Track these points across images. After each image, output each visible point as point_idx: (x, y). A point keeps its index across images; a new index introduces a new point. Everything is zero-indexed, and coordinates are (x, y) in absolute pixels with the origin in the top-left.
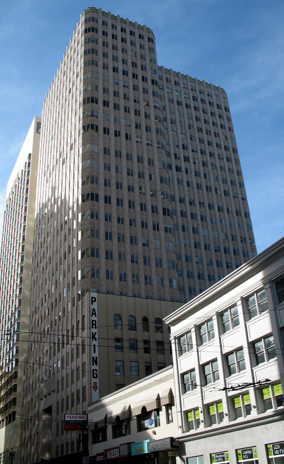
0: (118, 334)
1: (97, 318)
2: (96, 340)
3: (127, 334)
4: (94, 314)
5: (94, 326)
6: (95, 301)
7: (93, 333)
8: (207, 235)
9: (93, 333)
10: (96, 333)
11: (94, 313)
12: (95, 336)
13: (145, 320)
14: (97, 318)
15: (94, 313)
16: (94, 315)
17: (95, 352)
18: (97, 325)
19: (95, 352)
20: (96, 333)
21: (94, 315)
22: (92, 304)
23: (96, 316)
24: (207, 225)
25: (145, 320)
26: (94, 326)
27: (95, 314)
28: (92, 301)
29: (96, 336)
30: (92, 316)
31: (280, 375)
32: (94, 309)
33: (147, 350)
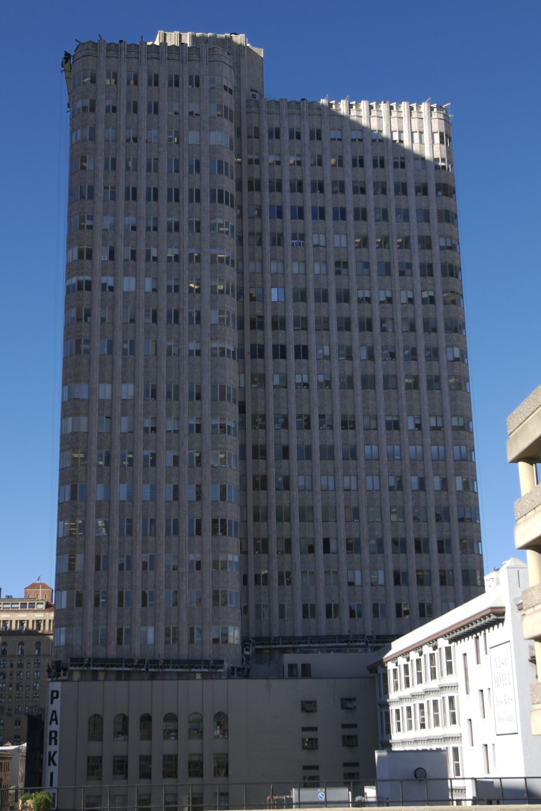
0: (95, 749)
1: (58, 726)
2: (54, 764)
3: (110, 748)
4: (54, 720)
5: (53, 741)
6: (57, 697)
7: (50, 753)
8: (354, 487)
9: (50, 753)
10: (55, 753)
11: (54, 717)
12: (54, 758)
13: (146, 719)
14: (58, 726)
15: (54, 717)
16: (54, 723)
17: (52, 774)
18: (58, 738)
19: (52, 774)
20: (55, 753)
21: (54, 723)
22: (52, 703)
23: (57, 723)
24: (357, 466)
25: (171, 718)
26: (53, 741)
27: (56, 720)
28: (52, 698)
29: (56, 758)
30: (51, 723)
31: (372, 787)
32: (54, 712)
33: (145, 774)
